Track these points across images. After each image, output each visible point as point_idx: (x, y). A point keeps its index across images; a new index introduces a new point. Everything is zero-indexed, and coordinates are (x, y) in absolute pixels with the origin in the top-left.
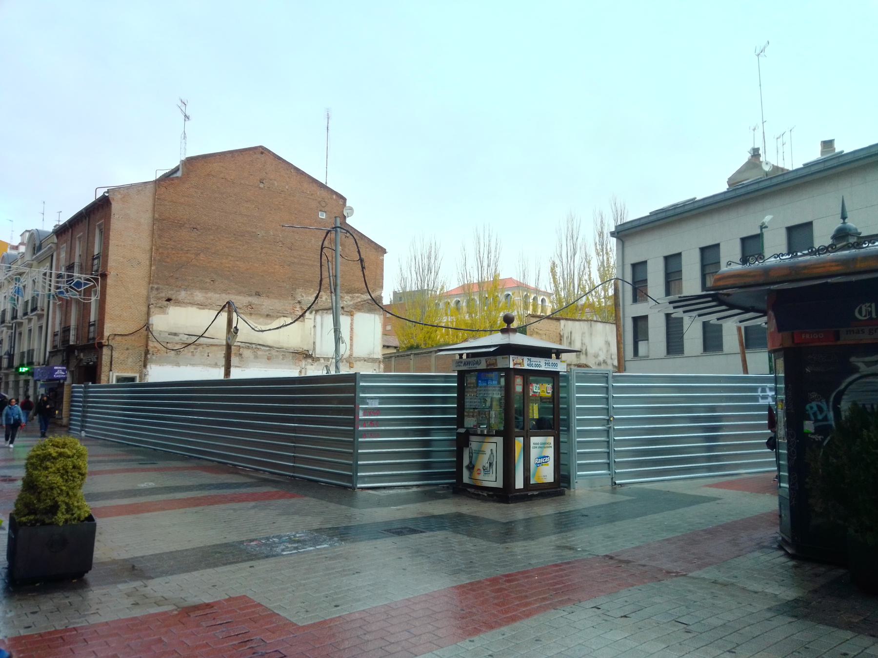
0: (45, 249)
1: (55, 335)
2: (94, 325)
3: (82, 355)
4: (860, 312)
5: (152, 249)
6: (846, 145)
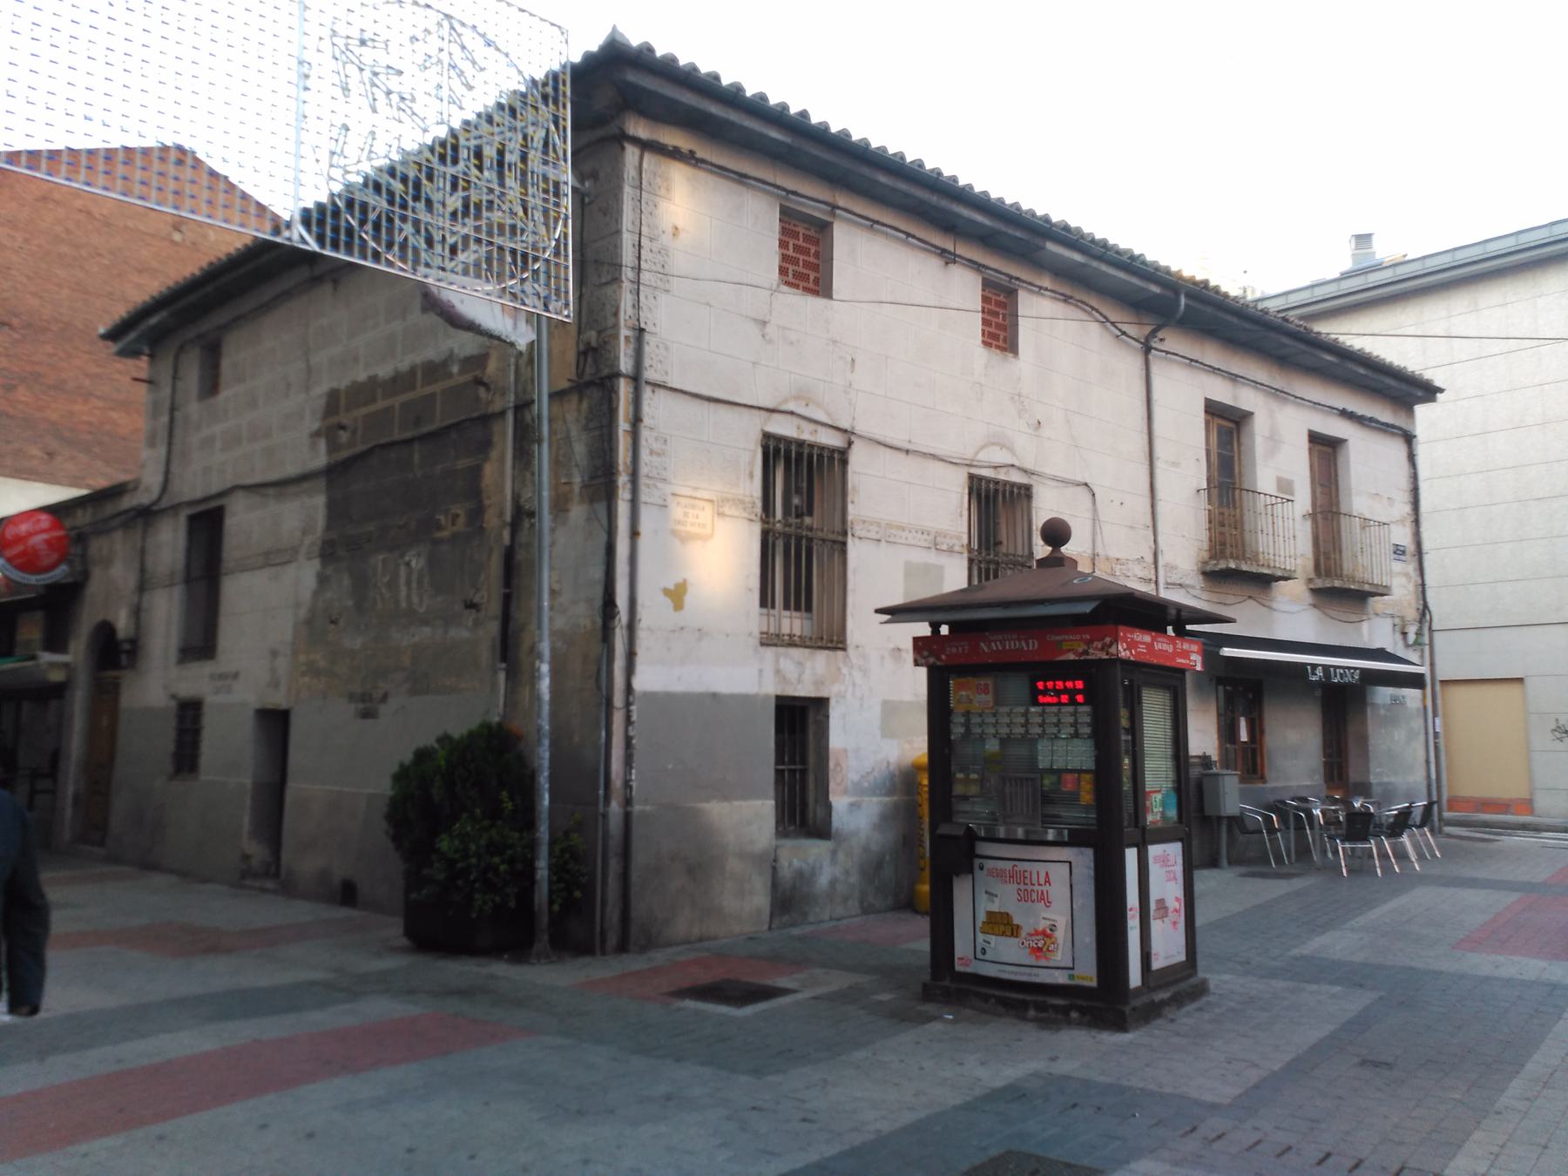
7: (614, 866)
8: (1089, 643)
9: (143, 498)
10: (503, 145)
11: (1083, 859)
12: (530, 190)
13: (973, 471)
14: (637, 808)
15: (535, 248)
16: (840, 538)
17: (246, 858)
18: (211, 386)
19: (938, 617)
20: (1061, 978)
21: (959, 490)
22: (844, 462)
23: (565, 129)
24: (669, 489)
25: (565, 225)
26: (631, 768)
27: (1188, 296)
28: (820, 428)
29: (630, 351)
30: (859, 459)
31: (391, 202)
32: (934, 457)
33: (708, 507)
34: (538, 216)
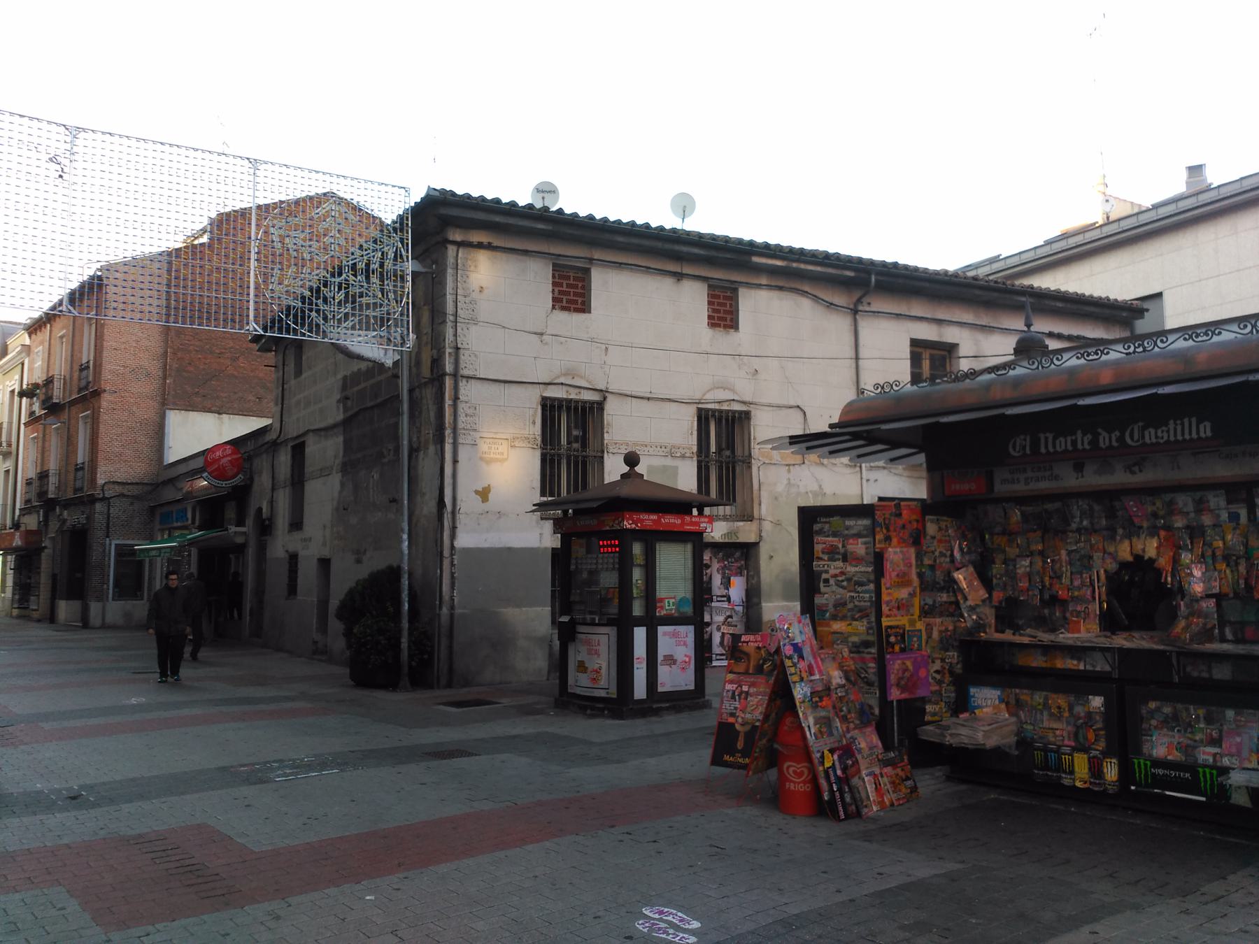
0: (14, 353)
1: (29, 483)
2: (82, 468)
3: (65, 513)
4: (1014, 448)
5: (166, 352)
6: (1220, 174)
7: (444, 642)
8: (614, 521)
9: (272, 436)
10: (369, 261)
11: (612, 631)
12: (386, 282)
13: (700, 406)
14: (458, 611)
15: (388, 314)
16: (599, 454)
17: (315, 643)
18: (298, 372)
19: (565, 507)
20: (602, 694)
21: (691, 419)
22: (602, 409)
23: (407, 244)
24: (477, 435)
25: (408, 298)
26: (454, 589)
27: (878, 273)
28: (582, 391)
29: (452, 360)
30: (611, 407)
31: (303, 303)
32: (670, 400)
33: (505, 443)
34: (391, 296)
